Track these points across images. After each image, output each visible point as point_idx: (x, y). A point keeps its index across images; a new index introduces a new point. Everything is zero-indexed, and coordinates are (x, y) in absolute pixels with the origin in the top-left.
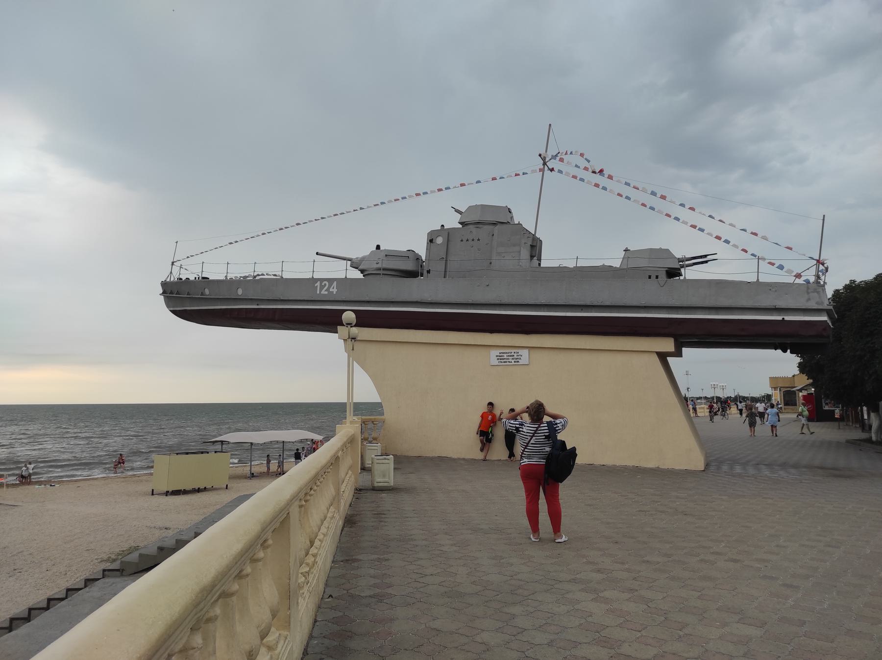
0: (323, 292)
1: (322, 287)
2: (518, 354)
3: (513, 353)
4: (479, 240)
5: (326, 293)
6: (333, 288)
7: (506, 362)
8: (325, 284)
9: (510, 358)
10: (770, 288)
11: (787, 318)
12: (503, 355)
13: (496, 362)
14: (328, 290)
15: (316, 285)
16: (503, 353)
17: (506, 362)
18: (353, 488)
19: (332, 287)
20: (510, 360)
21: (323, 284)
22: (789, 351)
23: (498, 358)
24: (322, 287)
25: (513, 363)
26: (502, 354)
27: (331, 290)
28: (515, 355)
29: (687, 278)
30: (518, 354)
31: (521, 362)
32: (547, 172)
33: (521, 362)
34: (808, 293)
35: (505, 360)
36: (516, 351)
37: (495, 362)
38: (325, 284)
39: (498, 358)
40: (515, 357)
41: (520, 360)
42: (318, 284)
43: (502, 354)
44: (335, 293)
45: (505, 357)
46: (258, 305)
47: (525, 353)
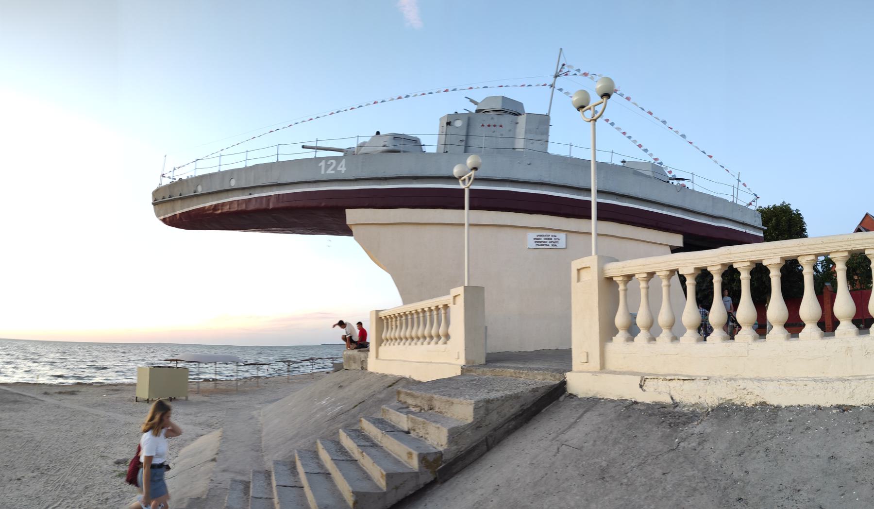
0: (328, 172)
1: (327, 167)
5: (333, 172)
6: (341, 167)
8: (332, 163)
12: (541, 237)
13: (533, 245)
14: (334, 169)
15: (320, 165)
16: (541, 236)
19: (340, 165)
21: (329, 163)
24: (327, 167)
26: (539, 237)
27: (339, 169)
28: (553, 238)
30: (556, 238)
31: (559, 246)
35: (542, 243)
36: (553, 234)
38: (332, 163)
40: (553, 240)
42: (323, 163)
43: (539, 237)
45: (543, 240)
46: (250, 194)
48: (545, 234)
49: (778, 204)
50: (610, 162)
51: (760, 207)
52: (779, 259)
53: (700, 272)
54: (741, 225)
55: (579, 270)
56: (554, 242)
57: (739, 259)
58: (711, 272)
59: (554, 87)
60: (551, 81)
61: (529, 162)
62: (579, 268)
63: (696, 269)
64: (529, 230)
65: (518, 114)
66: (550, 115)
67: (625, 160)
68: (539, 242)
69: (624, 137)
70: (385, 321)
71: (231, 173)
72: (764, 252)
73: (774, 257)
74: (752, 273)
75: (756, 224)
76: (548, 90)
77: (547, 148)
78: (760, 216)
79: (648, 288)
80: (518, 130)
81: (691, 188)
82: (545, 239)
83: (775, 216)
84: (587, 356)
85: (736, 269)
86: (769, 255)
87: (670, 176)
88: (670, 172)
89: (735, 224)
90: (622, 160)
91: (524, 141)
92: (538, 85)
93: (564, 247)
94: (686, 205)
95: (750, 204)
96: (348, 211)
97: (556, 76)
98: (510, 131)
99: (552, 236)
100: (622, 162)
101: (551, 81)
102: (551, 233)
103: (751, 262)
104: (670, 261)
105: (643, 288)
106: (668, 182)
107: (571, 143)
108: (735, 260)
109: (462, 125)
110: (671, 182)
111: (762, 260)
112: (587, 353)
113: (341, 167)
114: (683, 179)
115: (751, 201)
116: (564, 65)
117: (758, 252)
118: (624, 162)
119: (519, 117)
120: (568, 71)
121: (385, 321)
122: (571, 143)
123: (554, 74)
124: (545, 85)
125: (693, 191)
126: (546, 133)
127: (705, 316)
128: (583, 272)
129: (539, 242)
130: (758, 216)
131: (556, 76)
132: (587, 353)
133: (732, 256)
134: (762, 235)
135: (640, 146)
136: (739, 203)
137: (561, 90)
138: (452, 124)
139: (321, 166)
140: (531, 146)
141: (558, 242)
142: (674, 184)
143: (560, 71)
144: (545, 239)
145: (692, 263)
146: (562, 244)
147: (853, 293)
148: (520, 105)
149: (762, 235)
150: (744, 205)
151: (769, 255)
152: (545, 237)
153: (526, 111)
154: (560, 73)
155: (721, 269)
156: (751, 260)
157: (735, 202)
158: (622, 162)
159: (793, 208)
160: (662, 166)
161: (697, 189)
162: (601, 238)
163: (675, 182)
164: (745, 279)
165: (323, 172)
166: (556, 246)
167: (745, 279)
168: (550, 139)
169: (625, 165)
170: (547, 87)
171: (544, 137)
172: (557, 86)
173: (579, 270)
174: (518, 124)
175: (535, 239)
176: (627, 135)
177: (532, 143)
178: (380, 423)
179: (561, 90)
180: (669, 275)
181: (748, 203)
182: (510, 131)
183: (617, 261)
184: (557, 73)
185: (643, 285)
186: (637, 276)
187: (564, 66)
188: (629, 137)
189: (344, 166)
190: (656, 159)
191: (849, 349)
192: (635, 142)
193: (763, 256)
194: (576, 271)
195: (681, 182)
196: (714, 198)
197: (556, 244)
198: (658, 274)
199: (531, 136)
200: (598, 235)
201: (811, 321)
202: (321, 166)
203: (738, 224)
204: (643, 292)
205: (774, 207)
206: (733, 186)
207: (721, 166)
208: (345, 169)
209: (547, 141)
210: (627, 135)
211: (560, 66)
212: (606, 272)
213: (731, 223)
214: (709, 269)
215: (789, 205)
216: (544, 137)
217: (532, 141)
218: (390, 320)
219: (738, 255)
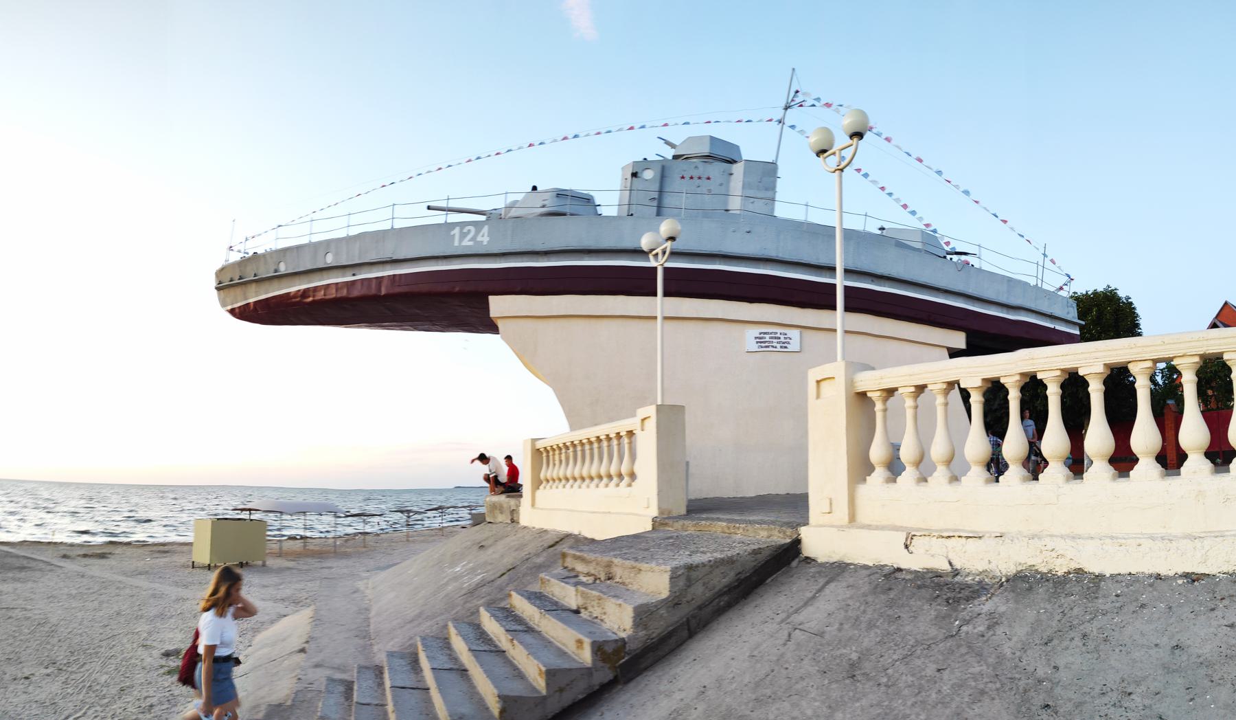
1: (463, 235)
2: (786, 336)
3: (779, 333)
4: (708, 178)
5: (471, 243)
6: (483, 236)
8: (469, 231)
9: (774, 340)
13: (755, 347)
14: (472, 239)
15: (452, 233)
16: (765, 333)
19: (481, 234)
20: (774, 344)
24: (463, 235)
26: (762, 335)
27: (479, 238)
28: (782, 337)
30: (786, 336)
31: (790, 348)
33: (790, 348)
35: (767, 344)
37: (754, 347)
38: (469, 231)
40: (782, 340)
42: (456, 231)
43: (762, 335)
44: (485, 243)
45: (767, 339)
46: (354, 275)
47: (794, 334)
48: (770, 331)
49: (1100, 289)
53: (990, 385)
56: (784, 343)
57: (1046, 367)
58: (1006, 385)
60: (779, 114)
61: (748, 230)
63: (984, 380)
65: (733, 162)
66: (778, 163)
67: (884, 226)
69: (883, 194)
70: (544, 454)
71: (327, 245)
73: (1095, 364)
74: (1063, 386)
75: (1069, 317)
77: (773, 209)
78: (1075, 305)
81: (977, 266)
82: (771, 338)
83: (1097, 305)
85: (1041, 380)
87: (947, 249)
88: (948, 243)
89: (1040, 317)
90: (880, 227)
91: (742, 200)
92: (760, 121)
93: (797, 349)
95: (1061, 288)
96: (492, 299)
97: (786, 108)
98: (721, 185)
99: (781, 334)
100: (880, 229)
101: (779, 114)
102: (779, 330)
103: (1062, 370)
105: (910, 407)
106: (945, 257)
107: (807, 203)
109: (653, 178)
110: (949, 257)
111: (1077, 368)
112: (831, 500)
113: (483, 236)
116: (797, 92)
118: (882, 229)
119: (735, 166)
120: (804, 101)
121: (544, 454)
123: (783, 105)
124: (771, 120)
125: (980, 270)
126: (772, 188)
127: (997, 447)
130: (1072, 306)
131: (786, 108)
132: (831, 500)
133: (1035, 361)
135: (905, 206)
136: (1045, 287)
137: (793, 127)
138: (639, 175)
139: (454, 235)
140: (751, 208)
141: (789, 343)
142: (953, 260)
143: (792, 100)
144: (771, 338)
146: (794, 345)
147: (1207, 414)
150: (1052, 289)
153: (744, 158)
154: (793, 103)
155: (1019, 381)
156: (1062, 367)
157: (1040, 285)
158: (880, 229)
159: (1122, 294)
160: (937, 235)
161: (986, 267)
163: (955, 258)
164: (1054, 395)
165: (456, 243)
166: (786, 347)
167: (1054, 395)
169: (884, 234)
170: (774, 124)
171: (769, 194)
172: (788, 122)
173: (818, 382)
175: (756, 338)
176: (887, 191)
177: (753, 203)
179: (793, 127)
180: (945, 389)
181: (1058, 287)
182: (721, 185)
183: (873, 369)
184: (787, 103)
185: (909, 403)
187: (798, 94)
188: (890, 194)
189: (486, 234)
190: (927, 225)
192: (898, 200)
194: (815, 384)
195: (963, 258)
196: (1010, 280)
197: (786, 345)
199: (751, 193)
202: (454, 235)
204: (909, 413)
205: (1095, 293)
207: (1019, 235)
208: (488, 239)
209: (773, 200)
210: (887, 191)
211: (792, 94)
214: (1002, 381)
216: (769, 194)
217: (752, 200)
218: (551, 453)
219: (1043, 361)
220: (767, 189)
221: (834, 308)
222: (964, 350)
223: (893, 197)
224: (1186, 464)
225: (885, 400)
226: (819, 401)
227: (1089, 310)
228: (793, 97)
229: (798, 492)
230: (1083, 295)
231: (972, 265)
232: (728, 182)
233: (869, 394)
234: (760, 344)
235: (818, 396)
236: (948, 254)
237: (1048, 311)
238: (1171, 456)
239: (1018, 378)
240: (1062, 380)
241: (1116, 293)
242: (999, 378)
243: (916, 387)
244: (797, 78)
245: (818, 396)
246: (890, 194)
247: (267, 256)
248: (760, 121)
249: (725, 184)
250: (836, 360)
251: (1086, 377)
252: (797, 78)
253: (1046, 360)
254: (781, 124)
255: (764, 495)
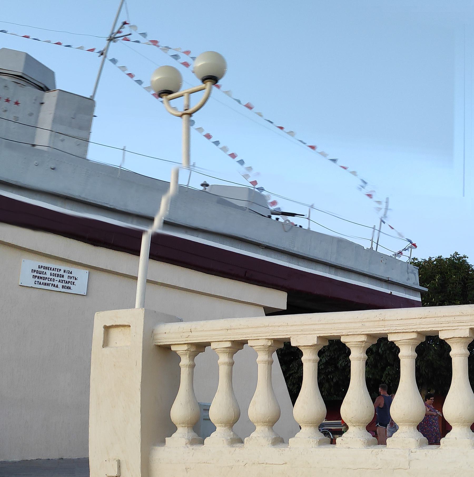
3: (62, 271)
7: (48, 285)
9: (56, 278)
10: (381, 259)
11: (394, 293)
12: (45, 271)
13: (30, 282)
16: (46, 268)
17: (48, 285)
18: (162, 221)
20: (56, 283)
22: (329, 297)
23: (35, 274)
25: (60, 289)
26: (42, 270)
28: (66, 275)
29: (311, 229)
30: (70, 275)
31: (74, 289)
32: (108, 63)
33: (74, 289)
34: (408, 273)
35: (46, 281)
36: (68, 268)
39: (35, 274)
40: (66, 278)
41: (72, 286)
43: (42, 270)
45: (48, 276)
48: (53, 266)
49: (446, 255)
50: (186, 184)
51: (414, 259)
52: (468, 331)
53: (327, 344)
54: (384, 284)
55: (107, 328)
57: (399, 329)
58: (347, 344)
59: (105, 57)
60: (101, 45)
61: (53, 166)
62: (108, 325)
63: (319, 338)
64: (26, 254)
65: (45, 89)
66: (95, 99)
67: (208, 183)
68: (41, 278)
69: (209, 143)
72: (443, 319)
73: (460, 328)
75: (410, 283)
76: (96, 59)
77: (86, 151)
78: (416, 271)
79: (232, 364)
80: (41, 115)
81: (305, 227)
83: (441, 273)
84: (119, 467)
85: (392, 343)
86: (451, 325)
87: (272, 208)
88: (274, 203)
89: (374, 281)
90: (202, 182)
91: (51, 135)
92: (81, 48)
93: (84, 292)
94: (296, 249)
95: (400, 253)
97: (112, 39)
98: (31, 114)
99: (65, 271)
100: (202, 185)
101: (101, 45)
102: (63, 267)
103: (419, 333)
104: (274, 326)
105: (224, 364)
106: (270, 217)
107: (125, 147)
108: (392, 329)
110: (274, 217)
111: (438, 332)
112: (119, 462)
114: (293, 215)
115: (401, 250)
116: (125, 23)
117: (433, 320)
118: (205, 185)
119: (47, 94)
120: (130, 34)
122: (125, 147)
123: (108, 35)
124: (92, 50)
125: (308, 231)
126: (87, 128)
128: (114, 333)
129: (41, 278)
130: (412, 272)
131: (112, 39)
132: (119, 462)
133: (386, 323)
134: (419, 299)
135: (233, 156)
136: (380, 250)
137: (114, 61)
140: (60, 145)
142: (280, 220)
143: (119, 32)
145: (314, 330)
148: (51, 74)
149: (419, 299)
150: (390, 254)
151: (451, 325)
152: (53, 272)
153: (59, 86)
154: (118, 35)
155: (366, 342)
156: (419, 330)
157: (374, 249)
158: (202, 185)
160: (264, 193)
161: (314, 228)
162: (151, 287)
163: (282, 219)
168: (91, 140)
169: (207, 190)
170: (95, 55)
171: (82, 134)
172: (110, 55)
173: (107, 328)
174: (43, 105)
175: (33, 271)
176: (213, 139)
177: (62, 140)
178: (312, 348)
179: (114, 61)
180: (270, 346)
181: (397, 251)
182: (31, 114)
183: (181, 320)
184: (113, 33)
185: (223, 359)
186: (213, 346)
187: (125, 26)
188: (217, 143)
190: (254, 183)
191: (357, 440)
192: (224, 149)
193: (440, 325)
194: (102, 330)
195: (290, 218)
196: (340, 241)
197: (69, 285)
198: (250, 343)
199: (61, 129)
200: (148, 281)
201: (357, 423)
203: (378, 282)
204: (223, 371)
205: (439, 260)
206: (374, 228)
209: (87, 141)
210: (213, 139)
211: (119, 24)
212: (159, 336)
213: (367, 279)
214: (343, 340)
215: (465, 257)
216: (82, 134)
217: (62, 137)
219: (397, 322)
220: (81, 128)
221: (137, 252)
222: (285, 310)
223: (221, 146)
224: (448, 435)
225: (193, 356)
226: (105, 349)
227: (433, 278)
228: (121, 28)
229: (75, 457)
230: (425, 261)
231: (301, 227)
232: (39, 112)
233: (173, 348)
234: (36, 279)
235: (106, 344)
236: (272, 214)
237: (385, 276)
238: (437, 427)
239: (364, 338)
240: (418, 343)
241: (465, 261)
242: (340, 337)
243: (233, 342)
244: (126, 8)
245: (106, 344)
246: (217, 143)
247: (333, 439)
248: (81, 48)
249: (35, 115)
250: (134, 307)
251: (447, 341)
252: (126, 8)
253: (401, 322)
254: (102, 56)
255: (31, 461)
